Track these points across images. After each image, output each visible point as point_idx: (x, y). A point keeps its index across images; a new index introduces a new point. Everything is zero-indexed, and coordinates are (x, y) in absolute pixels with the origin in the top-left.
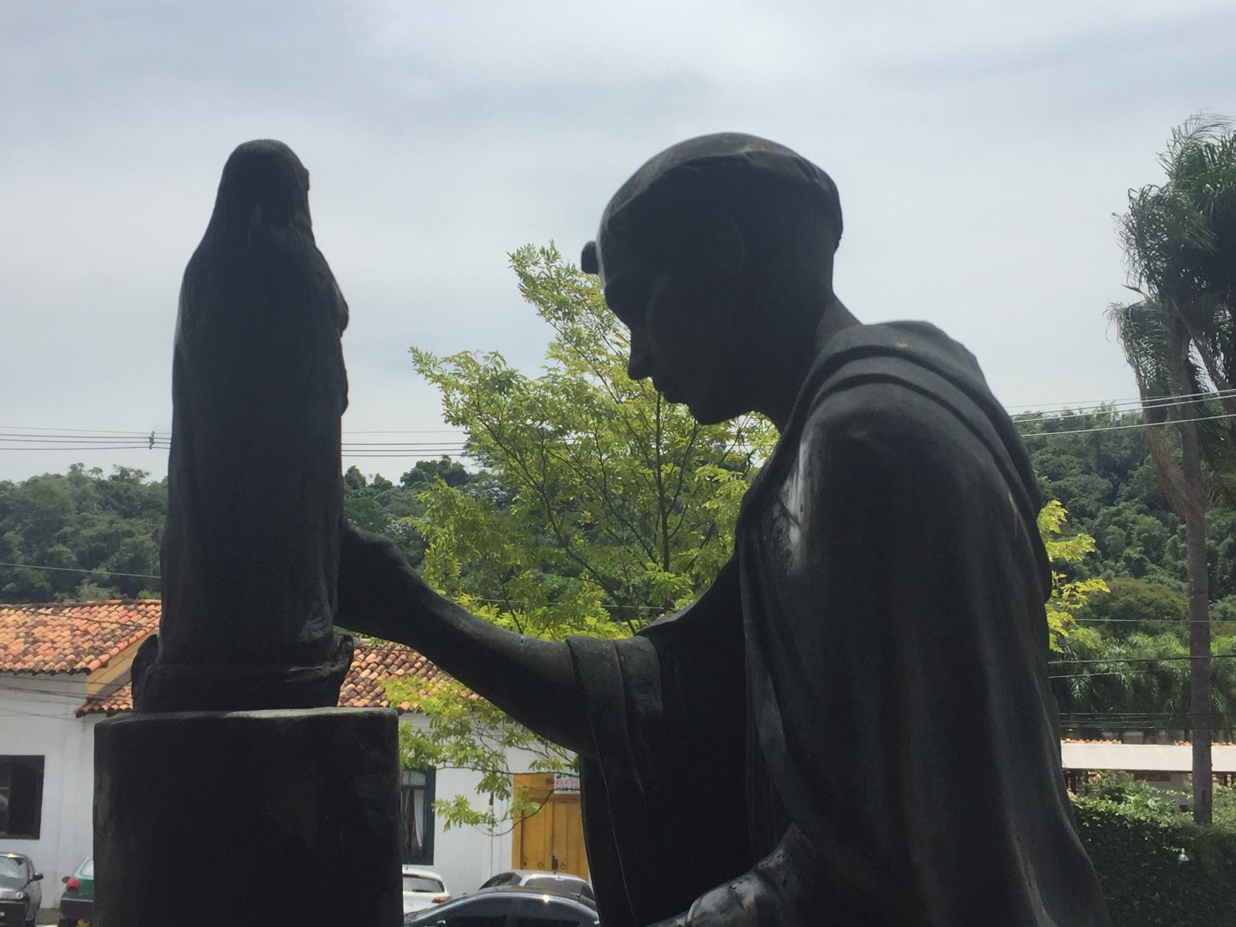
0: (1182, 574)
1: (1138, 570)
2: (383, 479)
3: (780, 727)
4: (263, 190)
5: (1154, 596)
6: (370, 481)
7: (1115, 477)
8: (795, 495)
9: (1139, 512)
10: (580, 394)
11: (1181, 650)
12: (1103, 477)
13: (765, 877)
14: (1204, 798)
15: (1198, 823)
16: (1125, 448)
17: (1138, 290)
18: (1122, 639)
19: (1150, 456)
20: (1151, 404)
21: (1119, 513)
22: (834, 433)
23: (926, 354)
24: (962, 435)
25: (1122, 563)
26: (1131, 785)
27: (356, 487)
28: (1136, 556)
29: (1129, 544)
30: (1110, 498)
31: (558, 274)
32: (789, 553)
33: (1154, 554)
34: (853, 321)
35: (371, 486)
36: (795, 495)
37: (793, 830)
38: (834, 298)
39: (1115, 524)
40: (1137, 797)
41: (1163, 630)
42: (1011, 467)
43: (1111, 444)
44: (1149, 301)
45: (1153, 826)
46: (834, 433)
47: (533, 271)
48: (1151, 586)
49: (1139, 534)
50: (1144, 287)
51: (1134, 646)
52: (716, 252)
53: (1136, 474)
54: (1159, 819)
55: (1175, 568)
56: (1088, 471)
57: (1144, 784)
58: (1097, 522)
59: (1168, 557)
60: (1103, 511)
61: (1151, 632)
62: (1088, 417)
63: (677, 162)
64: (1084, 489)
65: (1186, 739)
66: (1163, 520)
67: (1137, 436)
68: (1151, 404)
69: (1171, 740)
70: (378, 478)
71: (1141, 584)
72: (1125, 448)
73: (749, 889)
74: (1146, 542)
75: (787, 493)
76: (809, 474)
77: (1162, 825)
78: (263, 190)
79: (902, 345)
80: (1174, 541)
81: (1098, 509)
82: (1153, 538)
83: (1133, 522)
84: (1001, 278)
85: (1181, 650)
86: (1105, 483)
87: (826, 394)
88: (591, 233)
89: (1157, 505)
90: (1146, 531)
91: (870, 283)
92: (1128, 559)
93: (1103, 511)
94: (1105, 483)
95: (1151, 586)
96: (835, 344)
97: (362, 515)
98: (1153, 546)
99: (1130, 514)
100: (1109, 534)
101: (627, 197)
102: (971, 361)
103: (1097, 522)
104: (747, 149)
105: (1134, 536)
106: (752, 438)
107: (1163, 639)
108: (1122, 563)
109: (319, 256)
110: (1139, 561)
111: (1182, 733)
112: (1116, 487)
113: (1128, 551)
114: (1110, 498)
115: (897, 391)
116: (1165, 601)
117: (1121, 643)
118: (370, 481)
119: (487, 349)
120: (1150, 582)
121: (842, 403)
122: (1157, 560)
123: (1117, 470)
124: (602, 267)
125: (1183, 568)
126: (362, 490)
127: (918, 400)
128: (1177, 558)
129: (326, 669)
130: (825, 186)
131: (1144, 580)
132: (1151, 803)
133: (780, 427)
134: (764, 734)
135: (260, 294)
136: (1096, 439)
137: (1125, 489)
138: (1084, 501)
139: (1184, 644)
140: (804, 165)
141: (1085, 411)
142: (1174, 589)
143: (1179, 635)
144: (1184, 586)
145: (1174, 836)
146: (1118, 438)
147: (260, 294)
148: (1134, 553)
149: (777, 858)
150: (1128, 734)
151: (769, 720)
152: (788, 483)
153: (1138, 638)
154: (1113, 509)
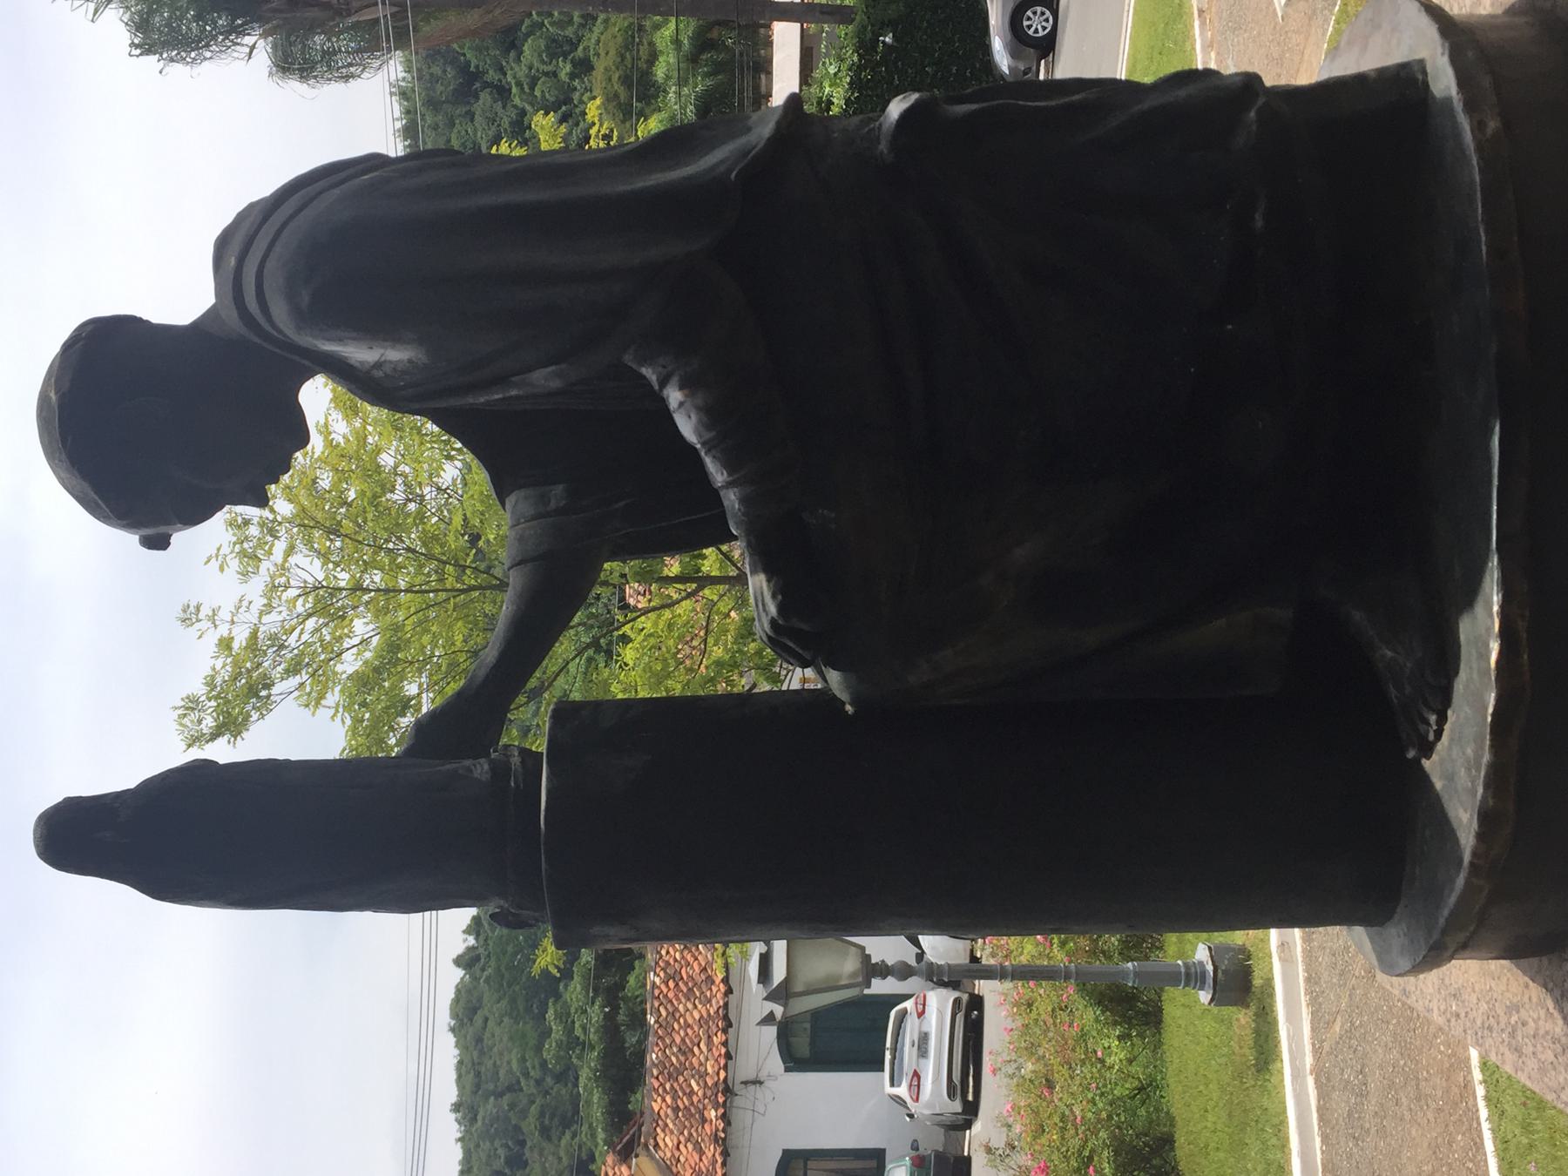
0: (589, 19)
1: (584, 67)
2: (469, 926)
3: (550, 369)
4: (83, 836)
5: (612, 52)
6: (471, 941)
7: (478, 85)
8: (361, 354)
9: (518, 60)
10: (364, 682)
11: (672, 25)
12: (477, 98)
13: (663, 382)
14: (828, 13)
15: (853, 20)
16: (445, 71)
17: (253, 48)
18: (661, 90)
19: (455, 46)
20: (388, 41)
21: (519, 84)
22: (309, 317)
23: (243, 246)
24: (309, 213)
25: (576, 83)
26: (814, 90)
27: (478, 958)
28: (568, 68)
29: (555, 74)
30: (502, 92)
31: (216, 698)
32: (410, 361)
33: (566, 48)
34: (214, 306)
35: (477, 939)
36: (361, 354)
37: (628, 359)
38: (195, 325)
39: (532, 88)
40: (826, 84)
41: (652, 44)
42: (343, 175)
43: (439, 88)
44: (264, 35)
45: (856, 70)
46: (309, 317)
47: (209, 723)
48: (603, 54)
49: (543, 62)
50: (249, 40)
51: (668, 77)
52: (150, 426)
53: (474, 62)
54: (849, 62)
55: (583, 26)
56: (471, 116)
57: (817, 74)
58: (528, 108)
59: (569, 32)
60: (517, 101)
61: (653, 57)
62: (408, 112)
63: (64, 456)
64: (492, 121)
65: (769, 27)
66: (528, 35)
67: (433, 55)
68: (388, 41)
69: (769, 44)
70: (467, 931)
71: (600, 66)
72: (445, 71)
73: (674, 396)
74: (553, 56)
75: (362, 363)
76: (340, 340)
77: (855, 58)
78: (83, 836)
79: (233, 261)
80: (552, 24)
81: (515, 107)
82: (548, 47)
83: (530, 68)
84: (181, 172)
85: (672, 25)
86: (485, 97)
87: (280, 331)
88: (128, 541)
89: (510, 41)
90: (540, 55)
91: (179, 293)
92: (572, 76)
93: (517, 101)
94: (485, 97)
95: (603, 54)
96: (231, 316)
97: (510, 949)
98: (558, 48)
99: (522, 72)
100: (543, 96)
101: (98, 505)
102: (251, 206)
103: (528, 108)
104: (53, 395)
105: (547, 68)
106: (317, 397)
107: (660, 45)
108: (576, 83)
109: (147, 785)
110: (574, 63)
111: (762, 31)
112: (486, 85)
113: (563, 75)
114: (502, 92)
115: (271, 264)
116: (620, 39)
117: (665, 91)
118: (471, 941)
119: (453, 1116)
120: (598, 55)
121: (280, 311)
122: (574, 46)
123: (469, 83)
124: (162, 529)
125: (582, 16)
126: (481, 950)
127: (278, 248)
128: (571, 22)
129: (516, 760)
130: (90, 328)
131: (594, 59)
132: (832, 70)
133: (311, 375)
134: (556, 384)
135: (178, 837)
136: (432, 104)
137: (492, 76)
138: (506, 123)
139: (666, 22)
140: (68, 347)
141: (397, 114)
142: (606, 28)
143: (657, 27)
144: (602, 16)
145: (866, 46)
146: (434, 79)
147: (178, 837)
148: (565, 69)
149: (650, 374)
150: (763, 90)
151: (544, 379)
152: (352, 362)
153: (660, 72)
154: (514, 90)
